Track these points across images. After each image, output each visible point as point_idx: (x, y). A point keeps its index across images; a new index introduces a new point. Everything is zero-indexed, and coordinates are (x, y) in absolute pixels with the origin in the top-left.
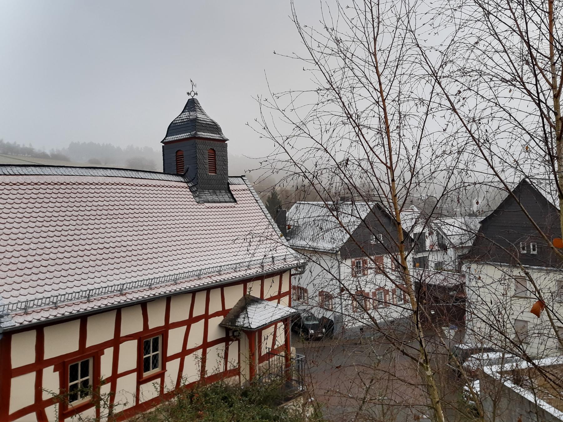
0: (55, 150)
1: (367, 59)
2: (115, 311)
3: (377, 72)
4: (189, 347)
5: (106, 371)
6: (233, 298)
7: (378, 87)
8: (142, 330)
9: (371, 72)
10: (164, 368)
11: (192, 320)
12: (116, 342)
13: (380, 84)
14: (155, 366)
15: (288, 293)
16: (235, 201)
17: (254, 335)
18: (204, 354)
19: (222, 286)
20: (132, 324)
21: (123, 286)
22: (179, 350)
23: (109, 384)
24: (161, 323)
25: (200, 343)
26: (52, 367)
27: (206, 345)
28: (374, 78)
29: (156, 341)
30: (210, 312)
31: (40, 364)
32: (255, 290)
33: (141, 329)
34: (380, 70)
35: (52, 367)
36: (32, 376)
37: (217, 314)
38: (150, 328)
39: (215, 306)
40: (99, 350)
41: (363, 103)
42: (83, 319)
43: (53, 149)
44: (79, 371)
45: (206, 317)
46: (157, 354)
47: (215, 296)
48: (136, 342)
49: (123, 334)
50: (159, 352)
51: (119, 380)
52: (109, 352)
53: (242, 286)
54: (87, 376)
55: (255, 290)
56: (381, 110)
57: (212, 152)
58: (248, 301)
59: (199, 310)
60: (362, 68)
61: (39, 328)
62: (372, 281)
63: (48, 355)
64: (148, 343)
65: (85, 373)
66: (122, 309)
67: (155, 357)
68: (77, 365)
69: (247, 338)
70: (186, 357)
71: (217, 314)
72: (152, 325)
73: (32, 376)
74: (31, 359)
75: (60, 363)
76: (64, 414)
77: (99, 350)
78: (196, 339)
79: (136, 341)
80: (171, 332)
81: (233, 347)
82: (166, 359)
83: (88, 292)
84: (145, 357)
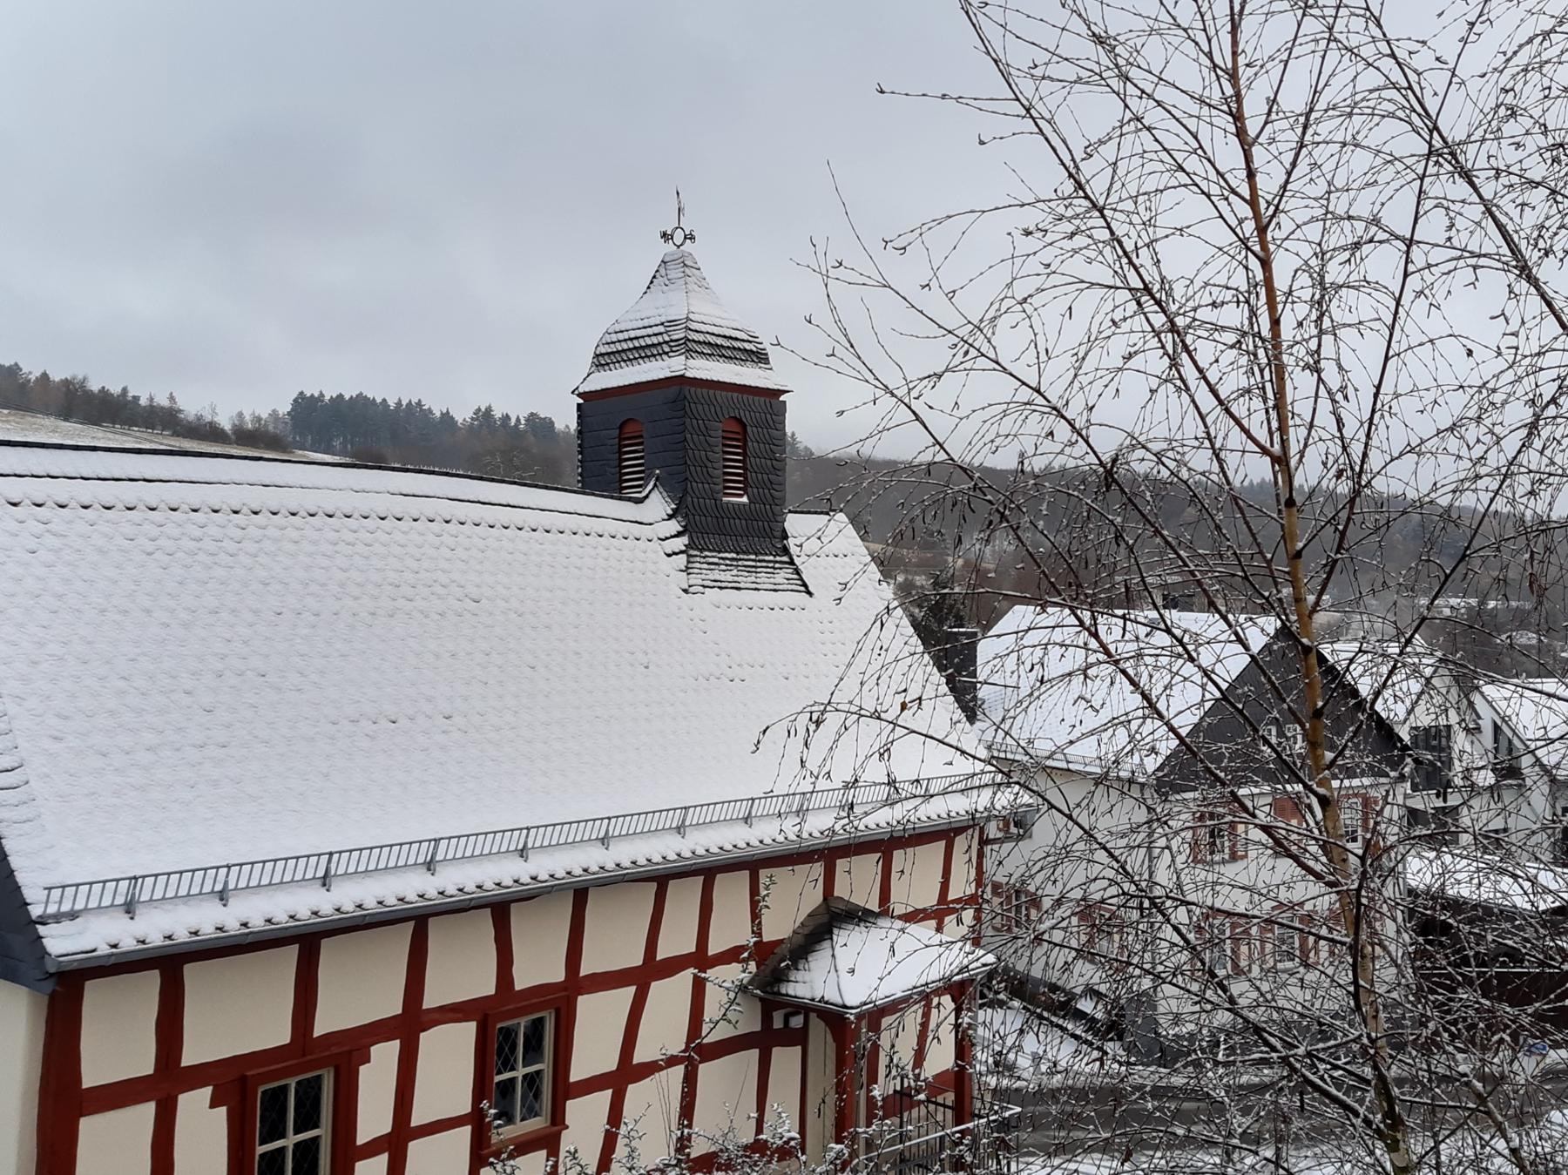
0: (248, 418)
1: (1207, 93)
2: (292, 952)
3: (1241, 133)
4: (639, 1057)
5: (373, 1120)
6: (790, 903)
7: (1245, 190)
8: (151, 1072)
9: (1218, 133)
10: (558, 1119)
11: (652, 970)
12: (409, 1025)
13: (1251, 175)
14: (530, 1112)
15: (972, 900)
16: (810, 593)
17: (847, 1034)
18: (690, 1080)
19: (754, 865)
20: (462, 972)
21: (436, 848)
22: (610, 1063)
23: (384, 1158)
24: (559, 975)
25: (677, 1046)
26: (207, 1091)
27: (698, 1052)
28: (1229, 155)
29: (537, 1028)
30: (714, 949)
31: (166, 1082)
32: (857, 881)
33: (488, 988)
34: (1252, 128)
35: (207, 1091)
36: (146, 1113)
37: (731, 956)
38: (520, 984)
39: (731, 929)
40: (351, 1049)
41: (1196, 252)
42: (307, 942)
43: (240, 415)
44: (521, 1043)
45: (701, 959)
46: (316, 1139)
47: (731, 894)
48: (471, 1027)
49: (431, 1000)
50: (545, 1066)
51: (414, 1147)
52: (386, 1054)
53: (818, 869)
54: (316, 1126)
55: (857, 881)
56: (1254, 264)
57: (737, 428)
58: (833, 917)
59: (677, 940)
60: (1192, 124)
61: (169, 965)
62: (1258, 878)
63: (189, 1058)
64: (509, 1034)
65: (308, 1119)
66: (90, 985)
67: (532, 1081)
68: (285, 1088)
69: (829, 1037)
70: (630, 1087)
71: (731, 956)
72: (523, 979)
73: (146, 1113)
74: (142, 1062)
75: (234, 1082)
76: (481, 1153)
77: (351, 1049)
78: (664, 1029)
79: (472, 1025)
80: (586, 1005)
81: (786, 1060)
82: (565, 1090)
83: (124, 885)
84: (497, 1078)
